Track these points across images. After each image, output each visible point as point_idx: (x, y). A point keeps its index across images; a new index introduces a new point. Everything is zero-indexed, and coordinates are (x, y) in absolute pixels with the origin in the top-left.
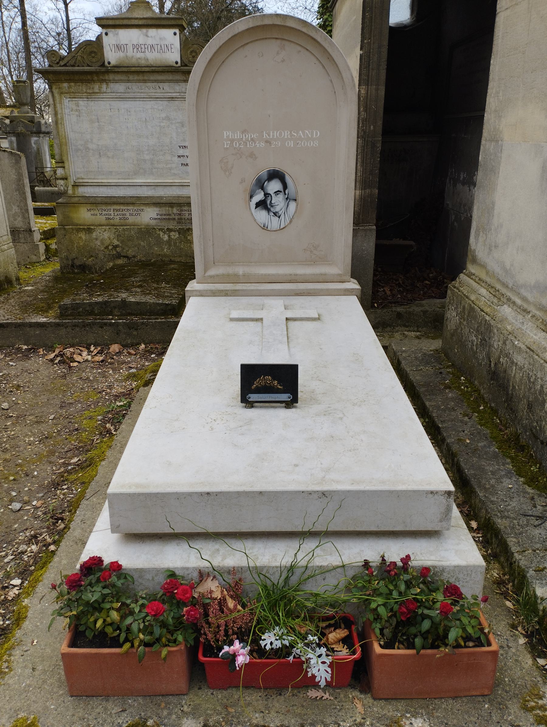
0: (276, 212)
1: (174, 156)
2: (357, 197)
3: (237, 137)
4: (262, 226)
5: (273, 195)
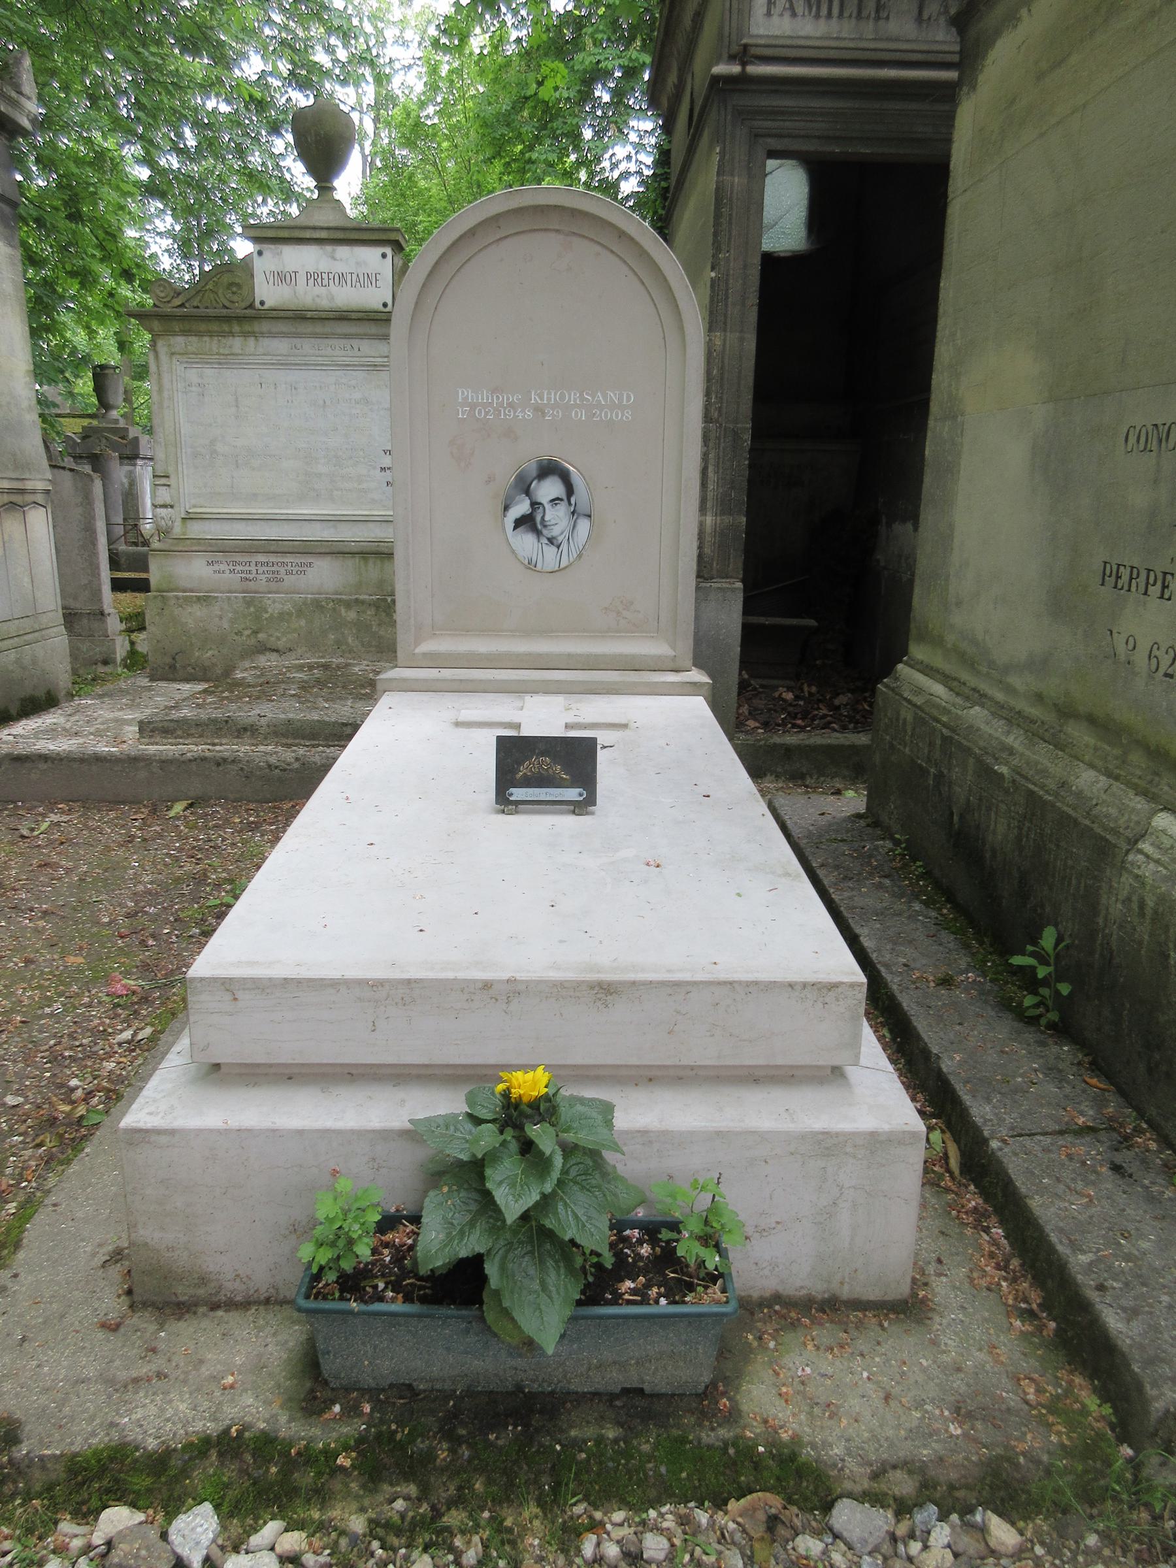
0: (554, 538)
1: (374, 468)
2: (708, 529)
4: (526, 562)
5: (547, 506)
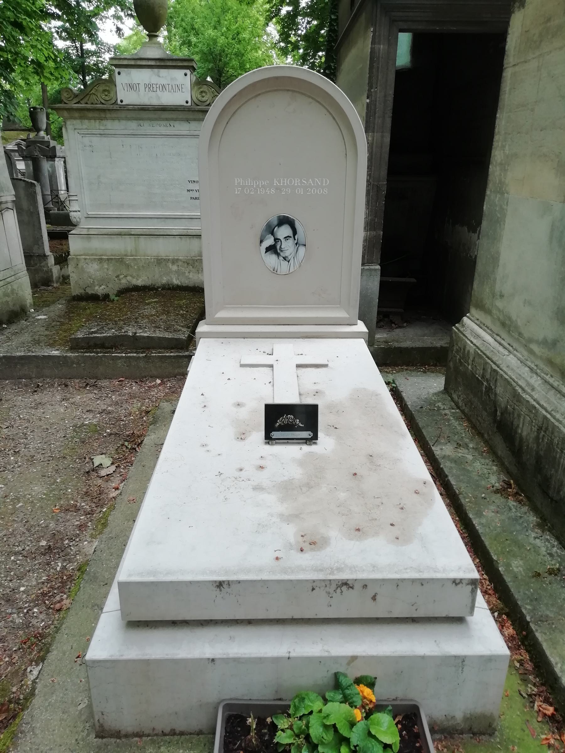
0: (286, 257)
3: (248, 183)
4: (272, 270)
5: (283, 240)
